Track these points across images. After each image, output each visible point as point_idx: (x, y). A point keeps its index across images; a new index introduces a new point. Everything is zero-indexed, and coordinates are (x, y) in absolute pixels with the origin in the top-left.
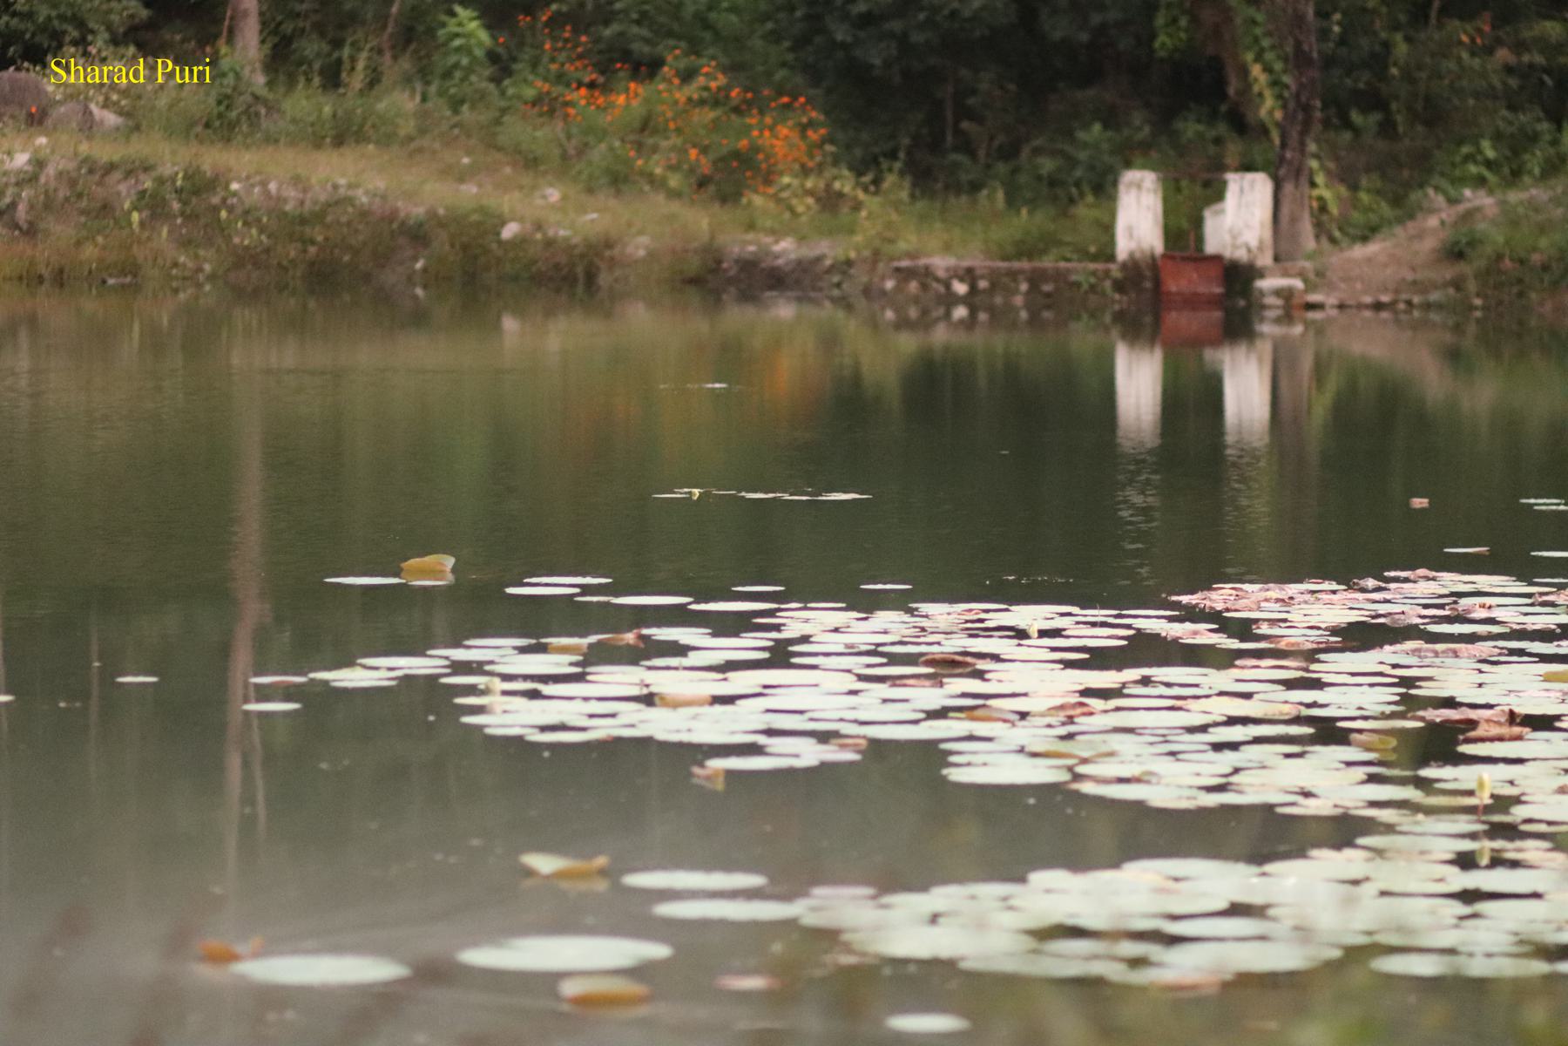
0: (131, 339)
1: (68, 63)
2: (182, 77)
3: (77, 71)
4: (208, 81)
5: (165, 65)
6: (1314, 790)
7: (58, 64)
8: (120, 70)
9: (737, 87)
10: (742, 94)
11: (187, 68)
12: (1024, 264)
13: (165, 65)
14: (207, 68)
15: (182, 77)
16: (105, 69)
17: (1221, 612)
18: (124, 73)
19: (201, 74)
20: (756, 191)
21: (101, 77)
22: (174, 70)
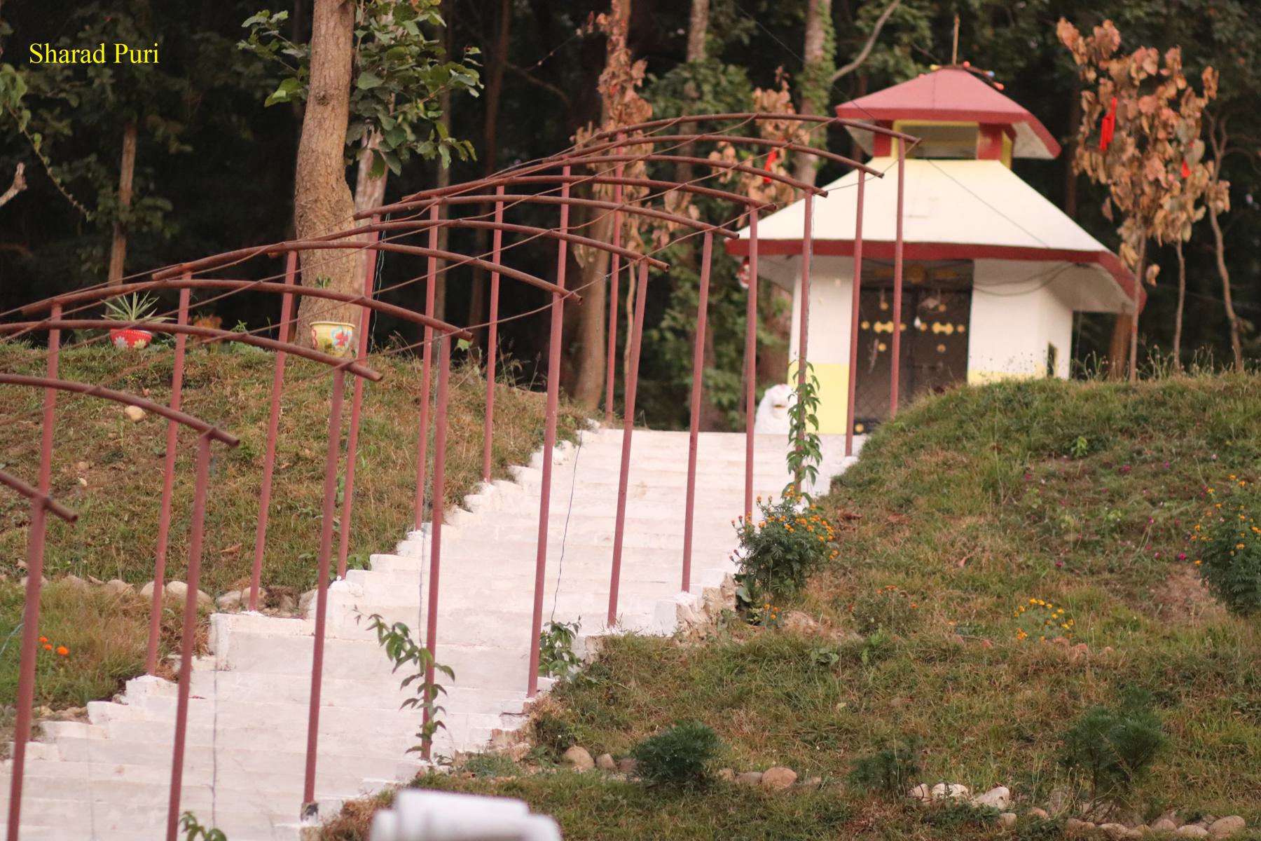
0: (116, 188)
1: (44, 47)
2: (136, 58)
3: (51, 55)
4: (156, 61)
5: (122, 49)
6: (1046, 348)
7: (36, 48)
8: (86, 53)
9: (579, 127)
10: (975, 124)
11: (139, 51)
12: (969, 556)
13: (122, 49)
14: (156, 51)
15: (136, 58)
16: (146, 52)
17: (324, 585)
18: (89, 55)
19: (151, 56)
20: (1098, 181)
21: (70, 58)
22: (129, 53)
